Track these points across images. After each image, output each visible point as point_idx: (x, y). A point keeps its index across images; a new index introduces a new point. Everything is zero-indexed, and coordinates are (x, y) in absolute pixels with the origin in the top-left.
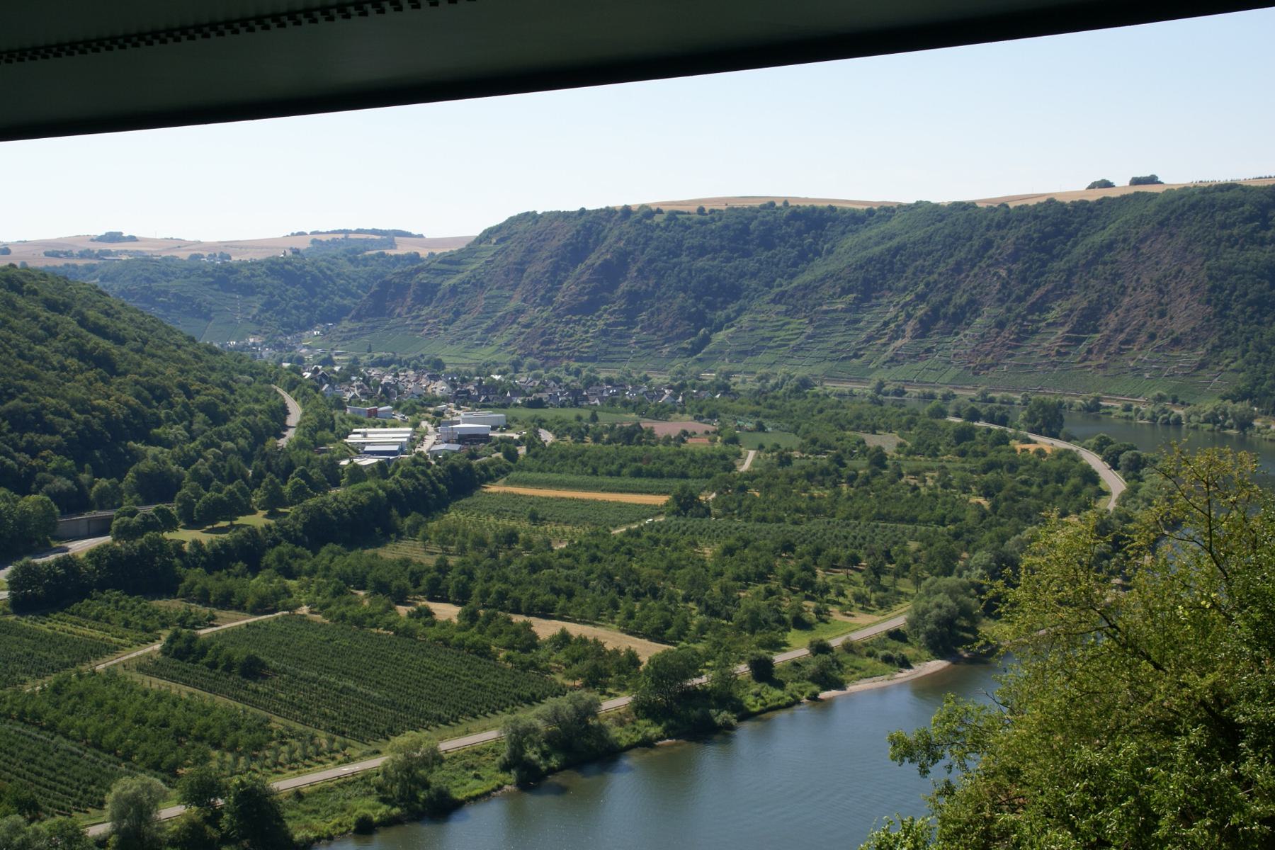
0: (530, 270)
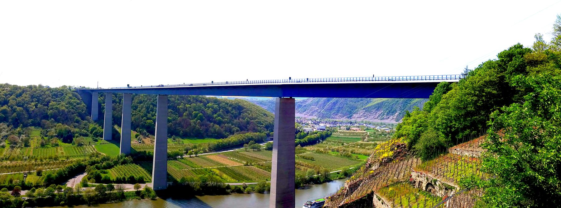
0: (320, 103)
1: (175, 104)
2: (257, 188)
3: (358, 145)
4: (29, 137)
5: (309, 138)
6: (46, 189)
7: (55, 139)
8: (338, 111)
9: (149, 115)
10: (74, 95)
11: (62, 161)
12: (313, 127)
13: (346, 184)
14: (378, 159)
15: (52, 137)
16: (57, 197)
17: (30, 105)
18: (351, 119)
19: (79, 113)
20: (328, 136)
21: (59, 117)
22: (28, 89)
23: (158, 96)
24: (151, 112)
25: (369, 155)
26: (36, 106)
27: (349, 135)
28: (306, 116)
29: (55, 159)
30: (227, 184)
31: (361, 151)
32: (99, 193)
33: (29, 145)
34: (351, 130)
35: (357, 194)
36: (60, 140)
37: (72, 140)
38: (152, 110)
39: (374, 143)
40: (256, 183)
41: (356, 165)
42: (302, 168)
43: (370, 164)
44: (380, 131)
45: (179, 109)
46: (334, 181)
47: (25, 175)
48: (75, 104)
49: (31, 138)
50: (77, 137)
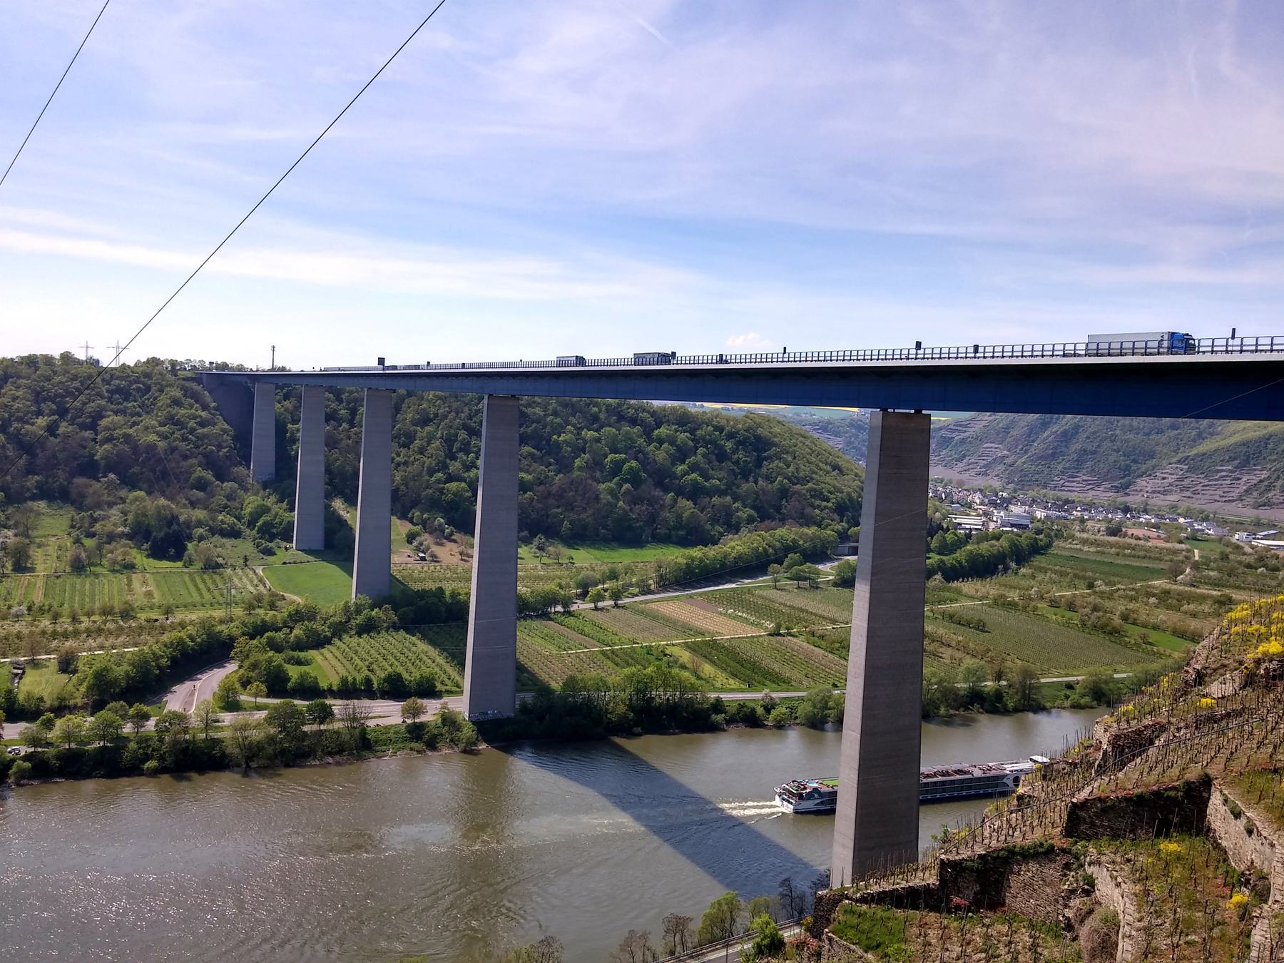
0: (1013, 433)
1: (544, 427)
2: (804, 709)
3: (1149, 595)
4: (27, 536)
5: (971, 552)
6: (92, 719)
7: (125, 546)
8: (1079, 464)
9: (454, 466)
10: (187, 392)
11: (148, 621)
12: (986, 514)
13: (1103, 729)
14: (1237, 657)
15: (111, 538)
16: (132, 745)
17: (33, 424)
18: (1127, 494)
19: (207, 456)
20: (1037, 549)
21: (136, 469)
22: (24, 370)
23: (486, 401)
24: (461, 455)
25: (1195, 638)
26: (52, 429)
27: (1118, 554)
28: (965, 476)
29: (122, 617)
30: (713, 695)
31: (1162, 616)
32: (280, 732)
33: (29, 565)
34: (1125, 535)
35: (1142, 773)
36: (139, 548)
37: (184, 548)
38: (466, 449)
39: (1219, 593)
40: (801, 694)
41: (1139, 668)
42: (947, 653)
43: (1198, 672)
44: (1250, 550)
45: (558, 445)
46: (1053, 710)
47: (16, 671)
48: (192, 424)
49: (37, 540)
50: (201, 539)
